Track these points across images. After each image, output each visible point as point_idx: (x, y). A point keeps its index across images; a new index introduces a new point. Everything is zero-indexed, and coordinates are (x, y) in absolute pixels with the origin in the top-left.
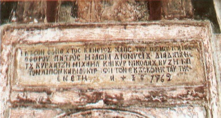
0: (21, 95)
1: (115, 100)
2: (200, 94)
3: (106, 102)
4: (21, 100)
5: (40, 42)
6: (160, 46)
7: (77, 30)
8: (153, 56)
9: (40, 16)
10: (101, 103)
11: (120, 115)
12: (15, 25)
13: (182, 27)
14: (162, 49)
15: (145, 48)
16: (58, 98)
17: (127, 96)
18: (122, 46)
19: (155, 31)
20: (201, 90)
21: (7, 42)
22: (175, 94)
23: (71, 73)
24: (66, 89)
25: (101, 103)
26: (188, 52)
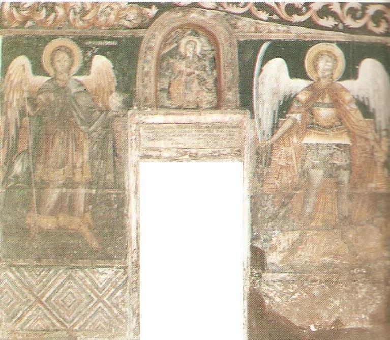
0: (145, 152)
1: (194, 155)
2: (239, 153)
3: (190, 156)
4: (146, 155)
5: (153, 123)
6: (219, 126)
7: (173, 116)
8: (215, 131)
9: (150, 107)
10: (187, 157)
11: (267, 105)
12: (137, 112)
13: (372, 309)
14: (219, 128)
15: (210, 126)
16: (165, 154)
17: (201, 153)
18: (198, 125)
19: (215, 117)
20: (239, 151)
21: (133, 122)
22: (225, 152)
23: (354, 106)
24: (168, 149)
25: (187, 157)
26: (235, 130)
